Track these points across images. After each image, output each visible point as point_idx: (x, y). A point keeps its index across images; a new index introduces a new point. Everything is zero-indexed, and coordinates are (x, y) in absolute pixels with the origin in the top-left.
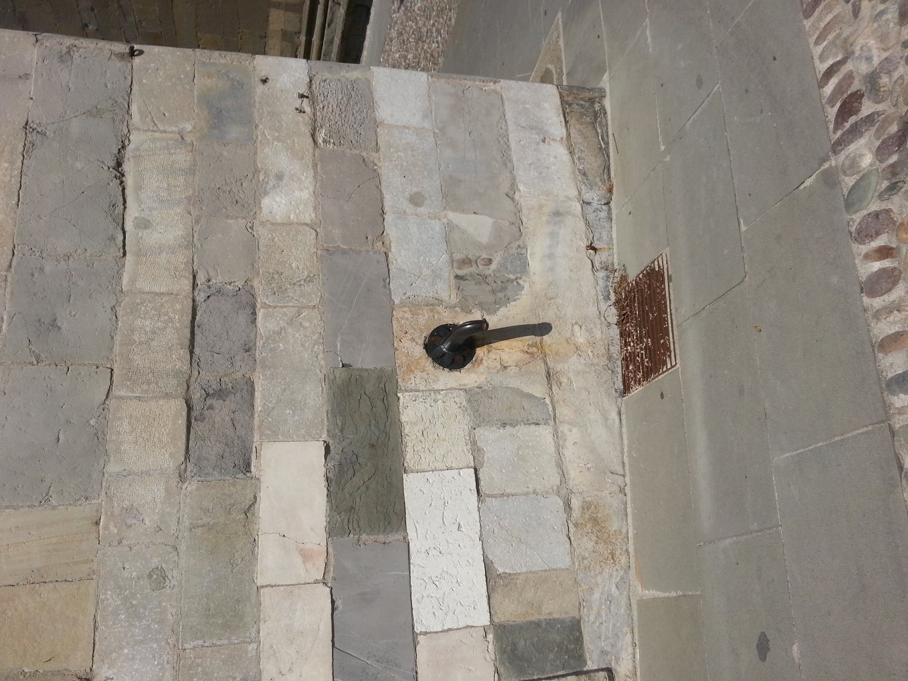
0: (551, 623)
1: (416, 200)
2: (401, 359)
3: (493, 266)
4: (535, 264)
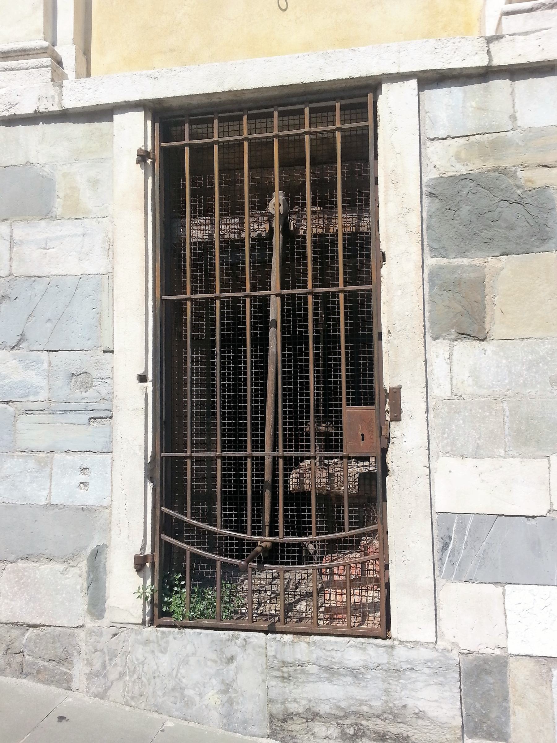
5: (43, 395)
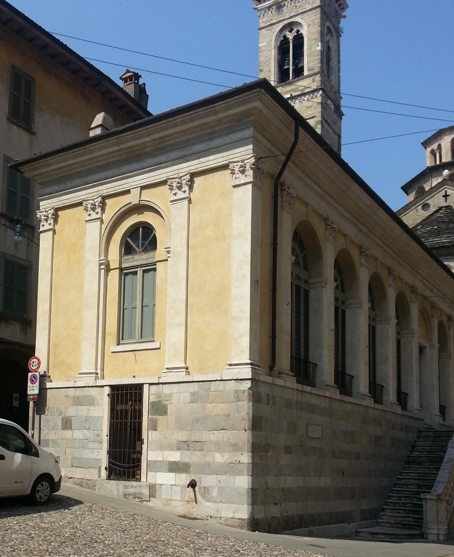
0: (156, 493)
1: (220, 482)
2: (192, 475)
3: (207, 495)
4: (208, 504)
5: (92, 438)
